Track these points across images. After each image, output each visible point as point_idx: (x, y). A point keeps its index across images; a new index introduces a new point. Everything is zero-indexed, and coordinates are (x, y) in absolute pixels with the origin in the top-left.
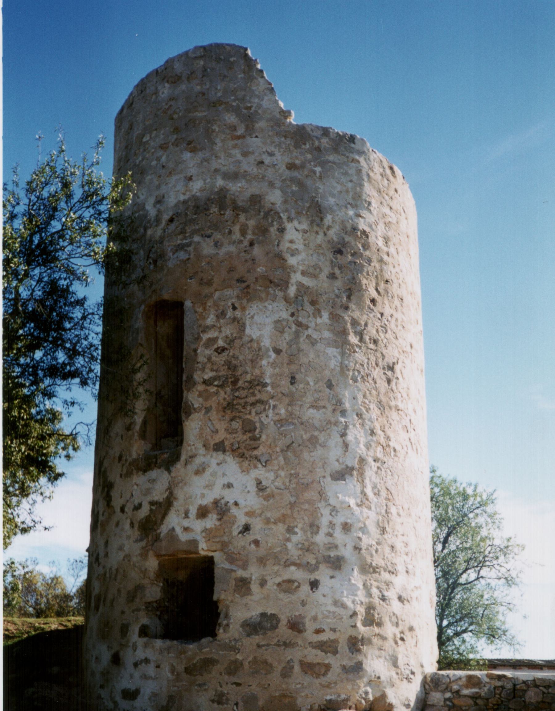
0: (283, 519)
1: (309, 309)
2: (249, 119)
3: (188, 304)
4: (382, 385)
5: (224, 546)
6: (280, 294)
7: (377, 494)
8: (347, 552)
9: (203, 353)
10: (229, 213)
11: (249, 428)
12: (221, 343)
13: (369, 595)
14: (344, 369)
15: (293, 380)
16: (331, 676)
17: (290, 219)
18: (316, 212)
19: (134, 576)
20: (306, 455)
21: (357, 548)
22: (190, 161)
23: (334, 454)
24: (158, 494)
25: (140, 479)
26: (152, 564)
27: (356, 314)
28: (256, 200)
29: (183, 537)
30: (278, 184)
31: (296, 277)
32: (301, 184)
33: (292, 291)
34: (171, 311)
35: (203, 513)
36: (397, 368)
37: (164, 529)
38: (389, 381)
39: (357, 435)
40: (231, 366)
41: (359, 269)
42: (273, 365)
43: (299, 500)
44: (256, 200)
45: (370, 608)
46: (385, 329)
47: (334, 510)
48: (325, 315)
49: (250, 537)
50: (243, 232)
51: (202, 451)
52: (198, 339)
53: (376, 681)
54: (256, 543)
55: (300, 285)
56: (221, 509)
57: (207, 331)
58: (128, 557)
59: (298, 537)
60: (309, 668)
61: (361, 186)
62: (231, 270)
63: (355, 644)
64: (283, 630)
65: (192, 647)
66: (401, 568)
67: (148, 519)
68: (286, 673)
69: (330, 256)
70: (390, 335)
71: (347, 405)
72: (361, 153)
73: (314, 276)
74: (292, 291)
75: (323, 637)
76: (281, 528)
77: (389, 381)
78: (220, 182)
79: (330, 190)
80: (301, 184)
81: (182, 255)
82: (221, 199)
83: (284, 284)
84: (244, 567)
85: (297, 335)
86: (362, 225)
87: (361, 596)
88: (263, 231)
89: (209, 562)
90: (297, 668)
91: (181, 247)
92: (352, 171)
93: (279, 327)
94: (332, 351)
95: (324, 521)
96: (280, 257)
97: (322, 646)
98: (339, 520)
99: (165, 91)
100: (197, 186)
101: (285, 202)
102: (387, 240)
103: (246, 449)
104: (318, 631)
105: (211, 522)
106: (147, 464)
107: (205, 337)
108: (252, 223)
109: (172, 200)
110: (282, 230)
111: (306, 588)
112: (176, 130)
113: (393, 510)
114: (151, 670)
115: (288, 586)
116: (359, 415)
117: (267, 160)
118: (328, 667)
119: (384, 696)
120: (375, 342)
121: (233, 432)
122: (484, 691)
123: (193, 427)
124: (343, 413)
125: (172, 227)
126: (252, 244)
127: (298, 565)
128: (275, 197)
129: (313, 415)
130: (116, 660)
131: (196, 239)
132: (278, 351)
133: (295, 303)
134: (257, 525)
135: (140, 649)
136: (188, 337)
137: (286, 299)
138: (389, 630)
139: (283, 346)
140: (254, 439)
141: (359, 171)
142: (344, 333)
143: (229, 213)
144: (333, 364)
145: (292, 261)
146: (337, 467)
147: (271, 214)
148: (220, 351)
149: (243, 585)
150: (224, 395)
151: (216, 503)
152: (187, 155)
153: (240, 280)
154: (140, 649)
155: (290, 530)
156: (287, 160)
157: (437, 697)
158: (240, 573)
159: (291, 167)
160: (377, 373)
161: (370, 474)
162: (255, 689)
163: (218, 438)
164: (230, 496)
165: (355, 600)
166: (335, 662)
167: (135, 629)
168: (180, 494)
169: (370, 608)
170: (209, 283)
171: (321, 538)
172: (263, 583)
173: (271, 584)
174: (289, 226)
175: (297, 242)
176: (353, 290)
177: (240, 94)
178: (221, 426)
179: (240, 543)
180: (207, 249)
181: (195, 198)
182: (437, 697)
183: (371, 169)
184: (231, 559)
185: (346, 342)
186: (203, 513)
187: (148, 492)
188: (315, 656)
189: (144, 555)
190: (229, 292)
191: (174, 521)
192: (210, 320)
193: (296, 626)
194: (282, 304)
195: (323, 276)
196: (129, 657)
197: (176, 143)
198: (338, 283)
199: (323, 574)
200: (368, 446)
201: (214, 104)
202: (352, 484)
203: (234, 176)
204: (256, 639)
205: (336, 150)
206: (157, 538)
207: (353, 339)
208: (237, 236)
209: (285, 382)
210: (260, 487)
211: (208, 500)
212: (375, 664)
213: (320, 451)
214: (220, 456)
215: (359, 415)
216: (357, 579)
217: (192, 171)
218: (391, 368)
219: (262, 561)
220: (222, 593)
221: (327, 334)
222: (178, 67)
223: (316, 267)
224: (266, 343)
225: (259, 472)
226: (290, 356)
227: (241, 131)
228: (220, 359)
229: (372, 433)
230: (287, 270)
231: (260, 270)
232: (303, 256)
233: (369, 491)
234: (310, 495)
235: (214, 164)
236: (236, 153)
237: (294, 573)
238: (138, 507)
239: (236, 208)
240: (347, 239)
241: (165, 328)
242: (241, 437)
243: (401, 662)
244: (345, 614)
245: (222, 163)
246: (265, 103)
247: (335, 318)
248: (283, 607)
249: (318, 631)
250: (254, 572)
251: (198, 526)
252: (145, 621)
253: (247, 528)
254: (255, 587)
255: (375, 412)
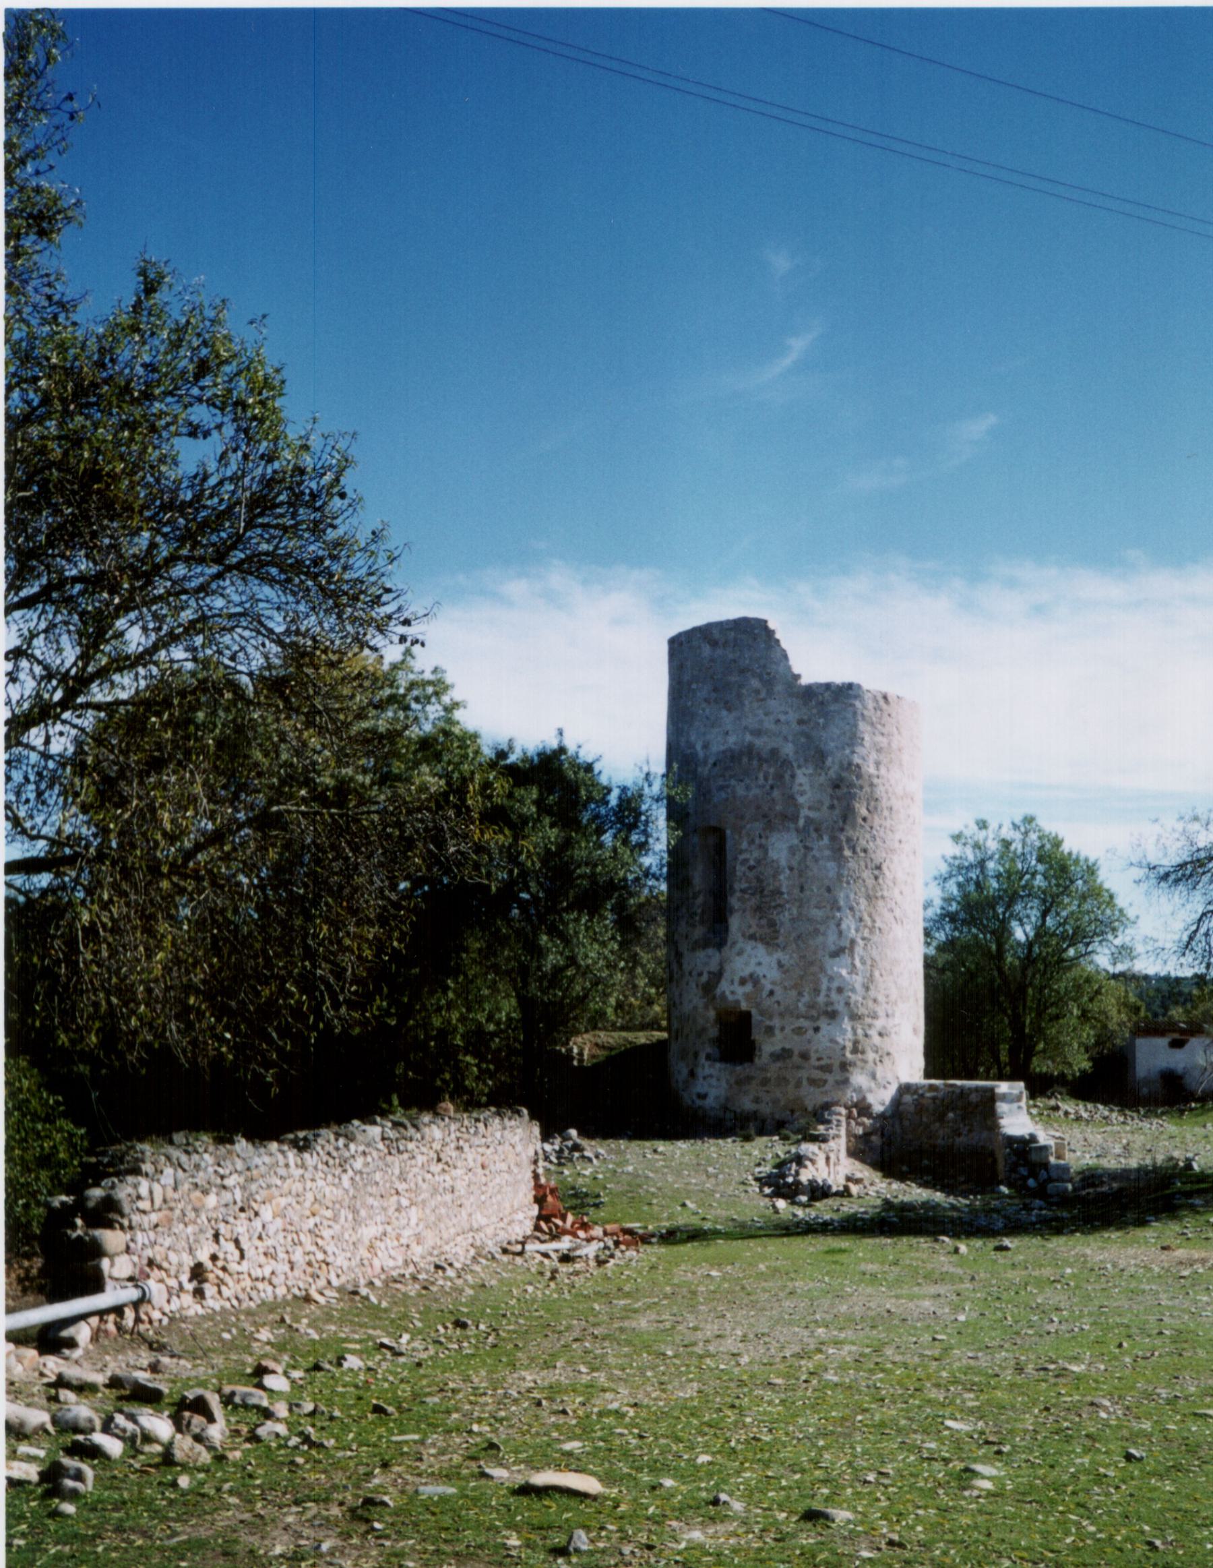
0: (795, 986)
1: (814, 835)
2: (769, 682)
3: (728, 832)
4: (870, 882)
5: (758, 1005)
6: (792, 826)
7: (863, 963)
8: (840, 1007)
9: (740, 870)
10: (755, 763)
11: (772, 924)
12: (752, 863)
13: (855, 1033)
14: (839, 876)
15: (802, 889)
16: (827, 1087)
17: (799, 767)
18: (819, 757)
19: (701, 1021)
20: (811, 942)
21: (847, 1004)
22: (727, 718)
23: (832, 938)
24: (714, 966)
25: (701, 955)
26: (712, 1014)
27: (851, 833)
28: (774, 752)
29: (730, 998)
30: (790, 738)
31: (804, 812)
32: (808, 736)
33: (801, 822)
34: (718, 834)
35: (743, 982)
36: (884, 867)
37: (718, 991)
38: (876, 878)
39: (849, 924)
40: (759, 880)
41: (852, 796)
42: (788, 878)
43: (807, 973)
44: (774, 752)
45: (856, 1043)
46: (874, 838)
47: (831, 979)
48: (826, 839)
49: (774, 999)
50: (766, 779)
51: (741, 939)
52: (736, 859)
53: (859, 1090)
54: (778, 1003)
55: (807, 818)
56: (754, 979)
57: (743, 853)
58: (695, 1008)
59: (806, 998)
60: (813, 1082)
61: (856, 726)
62: (758, 807)
63: (845, 1066)
64: (796, 1059)
65: (739, 1068)
66: (881, 1013)
67: (708, 983)
68: (798, 1085)
69: (830, 791)
70: (879, 841)
71: (842, 903)
72: (857, 697)
73: (819, 810)
74: (801, 822)
75: (822, 1063)
76: (794, 993)
77: (876, 878)
78: (748, 738)
79: (830, 738)
80: (808, 736)
81: (724, 795)
82: (749, 751)
83: (795, 819)
84: (771, 1018)
85: (805, 856)
86: (856, 760)
87: (849, 1035)
88: (779, 777)
89: (747, 1016)
90: (805, 1082)
91: (721, 788)
92: (849, 715)
93: (792, 850)
94: (831, 865)
95: (824, 987)
96: (792, 798)
97: (821, 1068)
98: (835, 985)
99: (707, 650)
100: (732, 739)
101: (796, 752)
102: (878, 764)
103: (769, 938)
104: (819, 1059)
105: (748, 988)
106: (705, 944)
107: (741, 857)
108: (772, 770)
109: (715, 748)
110: (793, 776)
111: (811, 1032)
112: (715, 690)
113: (877, 974)
114: (714, 1082)
115: (799, 1031)
116: (851, 909)
117: (783, 718)
118: (825, 1081)
119: (864, 1098)
120: (865, 851)
121: (761, 927)
122: (941, 1095)
123: (735, 922)
124: (839, 909)
125: (716, 769)
126: (772, 787)
127: (806, 1017)
128: (788, 750)
129: (817, 913)
130: (692, 1074)
131: (733, 782)
132: (791, 869)
133: (803, 833)
134: (778, 990)
135: (707, 1069)
136: (729, 857)
137: (797, 830)
138: (871, 1056)
139: (794, 863)
140: (777, 932)
141: (855, 713)
142: (841, 849)
143: (755, 763)
144: (832, 874)
145: (801, 800)
146: (833, 948)
147: (786, 763)
148: (751, 868)
149: (770, 1030)
150: (754, 901)
151: (751, 975)
152: (724, 713)
153: (765, 816)
154: (707, 1069)
155: (800, 994)
156: (797, 716)
157: (908, 1098)
158: (768, 1023)
159: (801, 722)
160: (866, 874)
161: (859, 950)
162: (779, 1095)
163: (752, 931)
164: (760, 971)
165: (846, 1039)
166: (831, 1078)
167: (702, 1056)
168: (727, 967)
169: (856, 1043)
170: (742, 817)
171: (821, 999)
172: (782, 1029)
173: (788, 1030)
174: (799, 772)
175: (807, 786)
176: (847, 815)
177: (762, 662)
178: (753, 922)
179: (768, 1003)
180: (740, 791)
181: (731, 750)
182: (908, 1098)
183: (865, 708)
184: (762, 1013)
185: (842, 856)
186: (743, 982)
187: (706, 964)
188: (817, 1074)
189: (706, 1007)
190: (757, 824)
191: (724, 986)
192: (744, 845)
193: (805, 1056)
194: (794, 834)
195: (825, 808)
196: (700, 1072)
197: (716, 701)
198: (837, 812)
199: (823, 1023)
200: (857, 930)
201: (742, 671)
202: (845, 959)
203: (758, 733)
204: (779, 1064)
205: (836, 700)
206: (714, 998)
207: (847, 853)
208: (761, 781)
209: (796, 891)
210: (780, 965)
211: (746, 973)
212: (859, 1079)
213: (820, 939)
214: (752, 943)
215: (851, 909)
216: (847, 1024)
217: (729, 727)
218: (879, 868)
219: (782, 1015)
220: (757, 1035)
221: (827, 853)
222: (716, 634)
223: (821, 802)
224: (783, 863)
225: (779, 955)
226: (800, 871)
227: (763, 695)
228: (751, 875)
229: (861, 920)
230: (797, 807)
231: (778, 808)
232: (809, 794)
233: (857, 963)
234: (814, 969)
235: (744, 723)
236: (760, 712)
237: (803, 1023)
238: (700, 974)
239: (760, 759)
240: (844, 774)
241: (712, 840)
242: (767, 930)
243: (878, 1075)
244: (838, 1048)
245: (750, 721)
246: (781, 669)
247: (833, 839)
248: (795, 1044)
249: (819, 1059)
250: (776, 1022)
251: (740, 991)
252: (709, 1050)
253: (772, 993)
254: (777, 1032)
255: (863, 902)
